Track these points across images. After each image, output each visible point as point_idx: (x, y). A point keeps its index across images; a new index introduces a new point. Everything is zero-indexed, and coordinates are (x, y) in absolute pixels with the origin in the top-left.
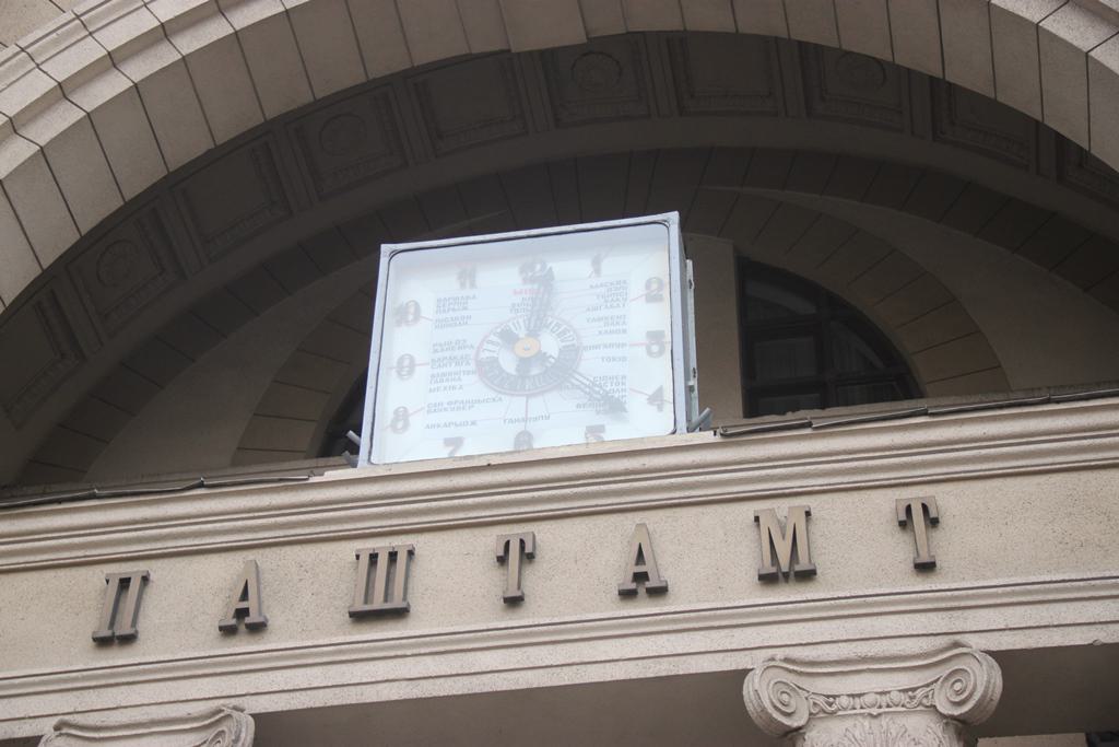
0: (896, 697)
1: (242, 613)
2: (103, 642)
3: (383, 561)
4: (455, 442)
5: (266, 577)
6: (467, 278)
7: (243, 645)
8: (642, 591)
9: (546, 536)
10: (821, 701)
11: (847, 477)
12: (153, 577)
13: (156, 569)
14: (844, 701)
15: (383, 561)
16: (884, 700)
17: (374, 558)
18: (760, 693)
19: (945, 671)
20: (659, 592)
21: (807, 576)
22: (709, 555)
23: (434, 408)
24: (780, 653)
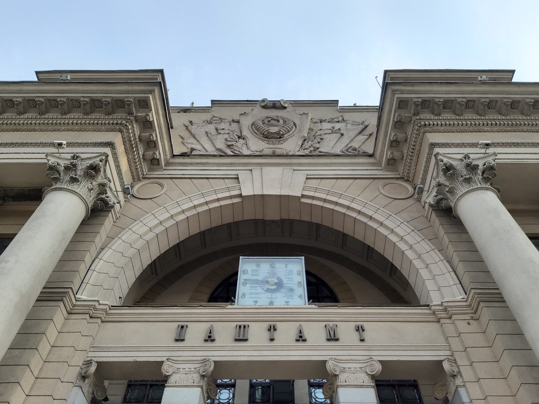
0: (192, 369)
1: (210, 337)
2: (177, 340)
3: (242, 327)
4: (256, 302)
5: (215, 329)
6: (258, 266)
7: (209, 344)
8: (301, 340)
9: (279, 325)
10: (342, 369)
11: (343, 317)
12: (188, 326)
13: (250, 324)
14: (347, 369)
15: (242, 327)
16: (355, 370)
17: (240, 327)
18: (330, 366)
19: (369, 364)
20: (305, 340)
21: (337, 340)
22: (315, 333)
23: (251, 294)
24: (333, 357)
